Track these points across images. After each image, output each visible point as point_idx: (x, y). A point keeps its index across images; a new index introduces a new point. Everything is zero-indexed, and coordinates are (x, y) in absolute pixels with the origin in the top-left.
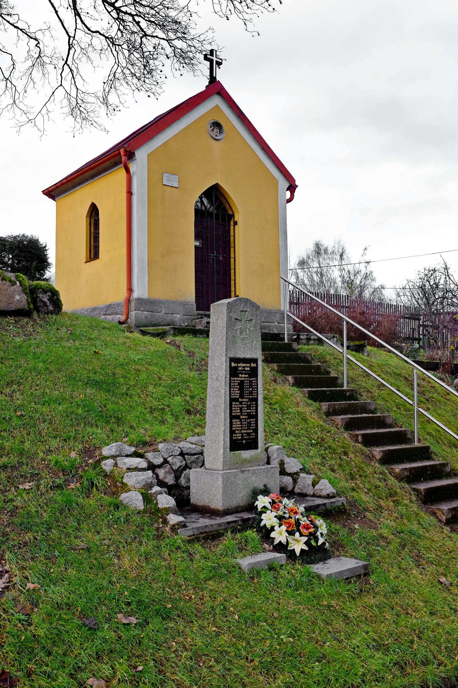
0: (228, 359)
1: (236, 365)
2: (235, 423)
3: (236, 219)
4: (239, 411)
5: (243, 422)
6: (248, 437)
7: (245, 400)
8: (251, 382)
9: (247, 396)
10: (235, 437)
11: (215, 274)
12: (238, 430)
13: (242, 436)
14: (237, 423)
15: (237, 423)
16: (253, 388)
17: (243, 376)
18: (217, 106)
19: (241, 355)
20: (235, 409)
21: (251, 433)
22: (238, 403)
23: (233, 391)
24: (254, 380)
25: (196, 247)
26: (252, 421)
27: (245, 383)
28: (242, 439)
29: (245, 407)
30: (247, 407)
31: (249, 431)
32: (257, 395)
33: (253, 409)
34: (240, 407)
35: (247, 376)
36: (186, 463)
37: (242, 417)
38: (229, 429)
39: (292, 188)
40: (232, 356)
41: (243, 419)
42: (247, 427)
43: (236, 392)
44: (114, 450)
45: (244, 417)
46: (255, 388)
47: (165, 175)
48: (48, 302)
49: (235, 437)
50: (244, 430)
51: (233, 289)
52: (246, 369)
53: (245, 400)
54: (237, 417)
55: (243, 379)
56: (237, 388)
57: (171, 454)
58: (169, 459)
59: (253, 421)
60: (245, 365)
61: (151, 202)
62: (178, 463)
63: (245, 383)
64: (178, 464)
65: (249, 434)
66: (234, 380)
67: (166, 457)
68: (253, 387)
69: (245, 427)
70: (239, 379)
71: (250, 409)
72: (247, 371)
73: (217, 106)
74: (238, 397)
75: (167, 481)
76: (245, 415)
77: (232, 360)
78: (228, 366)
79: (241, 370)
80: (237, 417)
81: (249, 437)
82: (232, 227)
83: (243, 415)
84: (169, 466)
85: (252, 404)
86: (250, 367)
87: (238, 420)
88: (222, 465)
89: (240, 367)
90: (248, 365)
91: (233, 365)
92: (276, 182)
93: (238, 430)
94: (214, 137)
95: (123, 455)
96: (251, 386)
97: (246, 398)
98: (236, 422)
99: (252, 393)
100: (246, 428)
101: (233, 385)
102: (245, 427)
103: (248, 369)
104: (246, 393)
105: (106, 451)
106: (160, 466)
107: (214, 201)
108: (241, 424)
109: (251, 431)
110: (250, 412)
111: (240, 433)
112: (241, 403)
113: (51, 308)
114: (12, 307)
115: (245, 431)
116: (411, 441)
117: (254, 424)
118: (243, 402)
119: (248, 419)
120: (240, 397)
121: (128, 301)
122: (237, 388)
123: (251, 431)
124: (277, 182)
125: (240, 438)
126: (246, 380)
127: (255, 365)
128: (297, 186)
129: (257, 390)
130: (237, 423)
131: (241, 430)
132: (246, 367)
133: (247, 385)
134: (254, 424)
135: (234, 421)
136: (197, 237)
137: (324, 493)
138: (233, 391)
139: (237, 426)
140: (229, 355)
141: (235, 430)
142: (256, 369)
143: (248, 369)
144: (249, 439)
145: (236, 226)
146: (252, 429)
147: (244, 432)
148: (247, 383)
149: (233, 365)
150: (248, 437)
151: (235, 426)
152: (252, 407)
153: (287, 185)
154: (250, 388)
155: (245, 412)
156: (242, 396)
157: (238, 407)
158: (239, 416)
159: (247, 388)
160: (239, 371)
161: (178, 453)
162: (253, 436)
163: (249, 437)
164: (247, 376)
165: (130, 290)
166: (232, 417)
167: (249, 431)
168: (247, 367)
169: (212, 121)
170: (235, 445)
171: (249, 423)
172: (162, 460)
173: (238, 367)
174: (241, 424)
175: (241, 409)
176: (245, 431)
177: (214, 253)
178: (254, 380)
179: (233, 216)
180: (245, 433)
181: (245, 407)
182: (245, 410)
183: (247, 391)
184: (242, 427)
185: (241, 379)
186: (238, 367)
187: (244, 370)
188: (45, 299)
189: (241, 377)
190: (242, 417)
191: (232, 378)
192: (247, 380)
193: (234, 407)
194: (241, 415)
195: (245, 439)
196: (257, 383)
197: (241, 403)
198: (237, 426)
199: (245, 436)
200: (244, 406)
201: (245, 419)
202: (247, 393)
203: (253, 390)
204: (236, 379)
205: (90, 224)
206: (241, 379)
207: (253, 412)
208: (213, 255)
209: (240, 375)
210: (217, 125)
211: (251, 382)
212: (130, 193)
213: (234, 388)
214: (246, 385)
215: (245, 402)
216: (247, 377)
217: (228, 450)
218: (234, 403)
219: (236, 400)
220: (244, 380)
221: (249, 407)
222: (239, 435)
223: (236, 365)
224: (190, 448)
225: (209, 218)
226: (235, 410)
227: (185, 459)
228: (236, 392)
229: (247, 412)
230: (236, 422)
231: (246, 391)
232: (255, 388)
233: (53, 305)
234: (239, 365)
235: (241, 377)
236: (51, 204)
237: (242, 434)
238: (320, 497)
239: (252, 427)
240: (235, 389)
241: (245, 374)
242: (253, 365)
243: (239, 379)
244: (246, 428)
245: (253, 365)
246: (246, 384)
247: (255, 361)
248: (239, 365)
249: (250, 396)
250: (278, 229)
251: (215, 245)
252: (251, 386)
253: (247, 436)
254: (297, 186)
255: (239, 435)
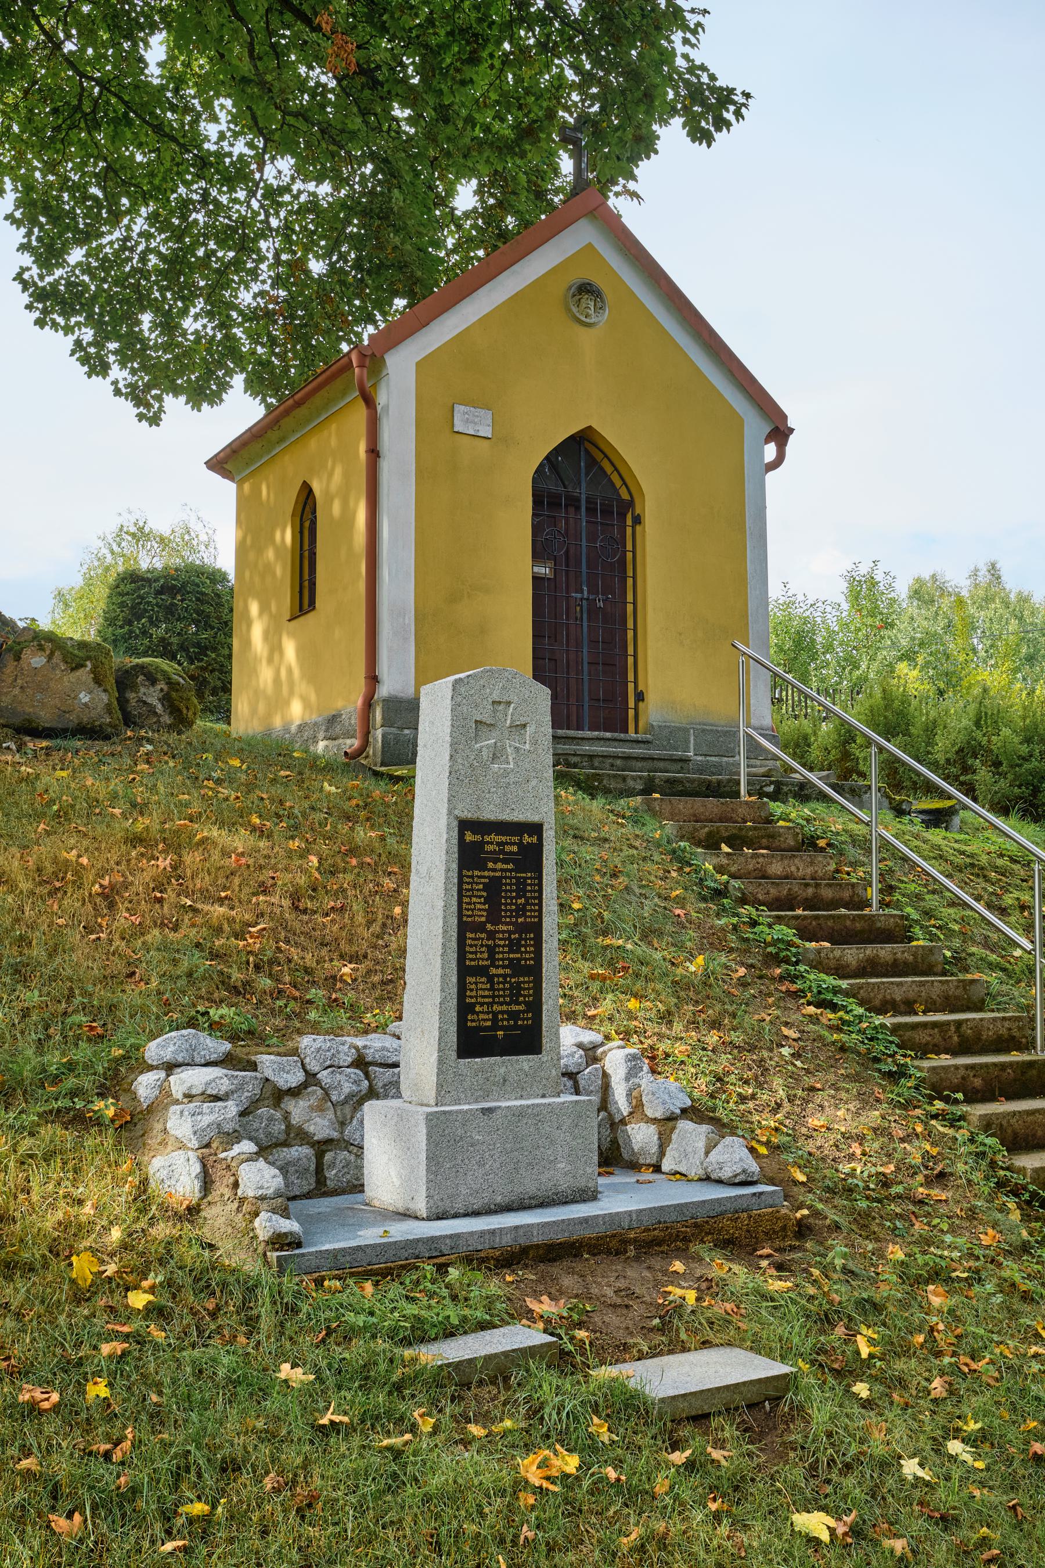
0: (455, 823)
1: (478, 838)
2: (473, 986)
3: (638, 511)
4: (486, 955)
5: (499, 983)
6: (512, 1022)
7: (505, 928)
8: (521, 884)
9: (510, 917)
10: (472, 1021)
11: (585, 643)
12: (482, 1004)
13: (495, 1020)
14: (480, 986)
15: (478, 986)
16: (527, 899)
17: (499, 865)
18: (590, 246)
19: (490, 813)
20: (473, 949)
21: (520, 1011)
22: (483, 935)
23: (469, 904)
24: (531, 878)
25: (537, 579)
26: (524, 982)
27: (506, 884)
28: (495, 1027)
29: (504, 946)
30: (510, 946)
31: (515, 1008)
32: (540, 917)
33: (526, 952)
34: (487, 946)
35: (511, 866)
36: (371, 1086)
37: (493, 971)
38: (455, 1001)
39: (780, 434)
40: (467, 815)
41: (498, 976)
42: (511, 995)
43: (478, 906)
44: (172, 1048)
45: (501, 971)
46: (535, 898)
47: (459, 409)
48: (159, 706)
49: (472, 1021)
50: (501, 1004)
51: (631, 677)
52: (507, 848)
53: (505, 928)
54: (481, 971)
55: (498, 874)
56: (480, 897)
57: (328, 1063)
58: (324, 1076)
59: (529, 982)
60: (504, 839)
61: (423, 474)
62: (347, 1084)
63: (506, 884)
64: (347, 1088)
65: (514, 1015)
66: (472, 877)
67: (316, 1069)
68: (528, 895)
69: (504, 996)
70: (486, 873)
71: (518, 951)
72: (511, 853)
73: (590, 246)
74: (483, 919)
75: (312, 1129)
76: (504, 967)
77: (465, 825)
78: (455, 841)
79: (494, 852)
80: (481, 971)
81: (516, 1023)
82: (629, 530)
83: (497, 967)
84: (320, 1092)
85: (526, 939)
86: (520, 844)
87: (484, 979)
88: (433, 1093)
89: (488, 843)
90: (516, 839)
91: (469, 837)
92: (739, 423)
93: (482, 1004)
94: (583, 318)
95: (197, 1060)
96: (521, 892)
97: (507, 924)
98: (476, 983)
99: (524, 910)
100: (508, 999)
101: (468, 890)
102: (504, 996)
103: (515, 849)
104: (506, 911)
105: (154, 1050)
106: (295, 1092)
107: (583, 471)
108: (492, 989)
109: (522, 1007)
110: (519, 960)
111: (488, 1013)
112: (491, 935)
113: (167, 719)
114: (72, 720)
115: (505, 1008)
116: (1029, 1045)
117: (529, 989)
118: (498, 932)
119: (511, 976)
120: (487, 921)
121: (369, 704)
122: (480, 897)
123: (522, 1007)
124: (741, 422)
125: (489, 1023)
126: (506, 878)
127: (535, 839)
128: (792, 430)
129: (540, 905)
130: (480, 986)
131: (491, 1004)
132: (507, 843)
133: (511, 891)
134: (529, 989)
135: (469, 979)
136: (537, 555)
137: (726, 1173)
138: (469, 904)
139: (480, 993)
140: (456, 812)
141: (474, 1005)
142: (538, 848)
143: (515, 849)
144: (516, 1027)
145: (638, 528)
146: (525, 1002)
147: (500, 1008)
148: (511, 884)
149: (469, 837)
150: (512, 1022)
151: (474, 993)
152: (525, 946)
153: (767, 429)
154: (518, 897)
155: (503, 959)
156: (494, 916)
157: (482, 946)
158: (487, 967)
159: (512, 898)
160: (488, 853)
161: (350, 1060)
162: (527, 1019)
163: (516, 1023)
164: (511, 866)
165: (373, 679)
166: (464, 971)
167: (515, 1008)
168: (511, 844)
169: (580, 281)
170: (473, 1040)
171: (518, 987)
172: (299, 1077)
173: (482, 843)
174: (492, 989)
175: (492, 951)
176: (505, 1008)
177: (582, 592)
178: (531, 878)
179: (631, 504)
180: (502, 1012)
181: (504, 946)
182: (503, 954)
183: (511, 904)
184: (493, 997)
185: (492, 874)
186: (482, 843)
187: (502, 852)
188: (153, 700)
189: (494, 870)
190: (493, 971)
191: (464, 872)
192: (511, 878)
193: (471, 946)
194: (493, 965)
195: (502, 1028)
196: (540, 885)
197: (491, 935)
198: (480, 993)
199: (502, 1020)
200: (502, 943)
201: (504, 976)
202: (511, 911)
203: (527, 903)
204: (476, 873)
205: (301, 532)
206: (492, 874)
207: (526, 960)
208: (579, 595)
209: (490, 865)
210: (586, 289)
211: (521, 884)
212: (374, 453)
213: (470, 897)
214: (506, 891)
215: (503, 932)
216: (511, 871)
217: (454, 1055)
218: (473, 936)
219: (480, 927)
220: (501, 877)
221: (514, 946)
222: (486, 1017)
223: (478, 838)
224: (383, 1049)
225: (572, 510)
226: (476, 953)
227: (367, 1076)
228: (478, 906)
229: (508, 959)
230: (476, 983)
231: (506, 904)
232: (535, 898)
233: (171, 713)
234: (487, 838)
235: (494, 870)
236: (227, 489)
237: (495, 1014)
238: (719, 1182)
239: (525, 996)
240: (474, 899)
241: (505, 861)
242: (527, 839)
243: (486, 873)
244: (508, 999)
245: (527, 839)
246: (508, 886)
247: (536, 829)
248: (487, 838)
249: (517, 916)
250: (737, 531)
251: (584, 574)
252: (521, 892)
253: (508, 1020)
254: (792, 430)
255: (486, 1017)
